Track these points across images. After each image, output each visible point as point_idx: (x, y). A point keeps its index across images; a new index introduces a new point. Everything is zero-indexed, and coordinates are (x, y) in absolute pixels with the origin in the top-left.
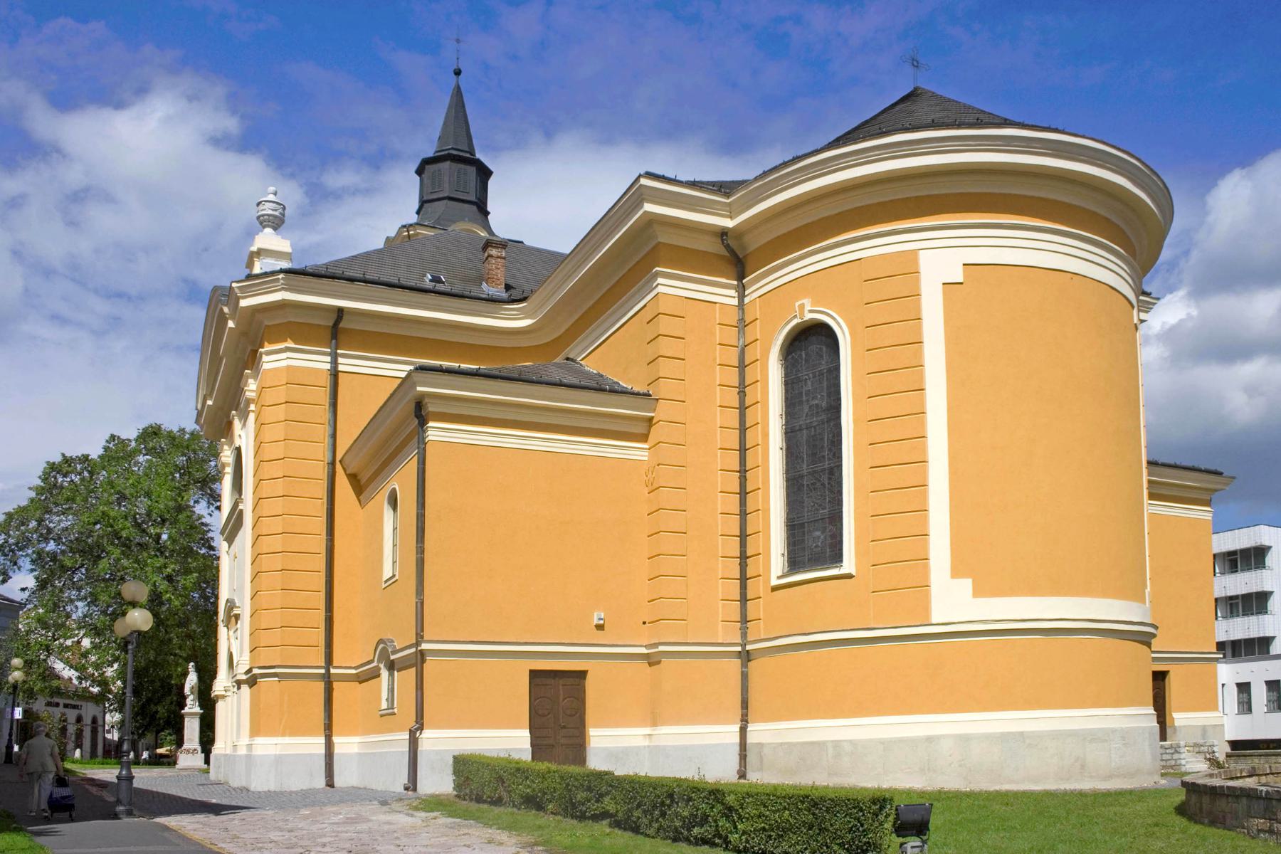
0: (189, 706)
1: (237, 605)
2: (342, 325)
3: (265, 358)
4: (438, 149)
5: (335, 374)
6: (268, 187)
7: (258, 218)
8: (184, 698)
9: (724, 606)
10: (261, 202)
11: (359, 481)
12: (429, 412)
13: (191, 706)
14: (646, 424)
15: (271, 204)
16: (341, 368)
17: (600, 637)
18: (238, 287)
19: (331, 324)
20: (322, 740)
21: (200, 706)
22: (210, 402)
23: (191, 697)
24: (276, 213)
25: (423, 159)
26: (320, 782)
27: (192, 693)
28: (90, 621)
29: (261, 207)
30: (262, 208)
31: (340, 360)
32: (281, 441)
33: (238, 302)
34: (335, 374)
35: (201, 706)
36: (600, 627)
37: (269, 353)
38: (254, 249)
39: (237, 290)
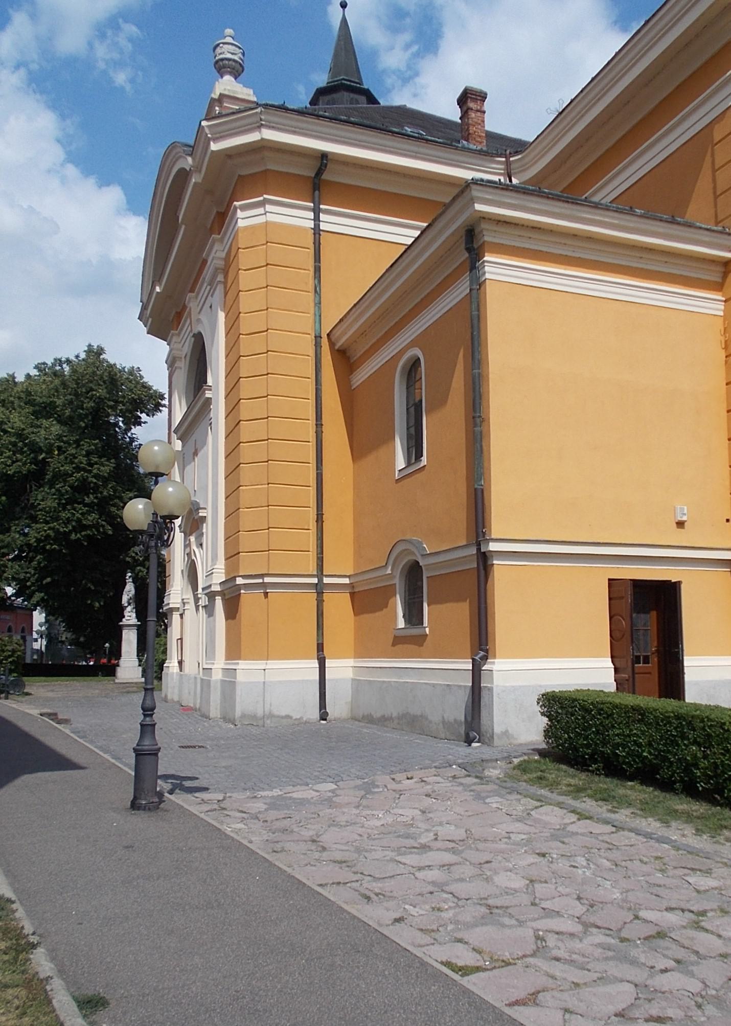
0: (127, 618)
1: (201, 506)
2: (325, 176)
3: (240, 214)
4: (330, 80)
5: (317, 231)
6: (226, 28)
7: (217, 62)
8: (123, 609)
9: (309, 526)
10: (218, 45)
11: (348, 358)
12: (484, 242)
13: (129, 618)
14: (722, 269)
15: (230, 47)
16: (323, 226)
17: (680, 537)
18: (208, 126)
19: (312, 174)
20: (315, 664)
21: (137, 617)
22: (158, 289)
23: (129, 609)
24: (236, 58)
25: (317, 89)
26: (315, 714)
27: (129, 604)
28: (74, 523)
29: (218, 50)
30: (220, 51)
31: (322, 217)
32: (264, 310)
33: (209, 144)
34: (317, 231)
35: (138, 617)
36: (680, 524)
37: (244, 208)
38: (215, 95)
39: (207, 131)
